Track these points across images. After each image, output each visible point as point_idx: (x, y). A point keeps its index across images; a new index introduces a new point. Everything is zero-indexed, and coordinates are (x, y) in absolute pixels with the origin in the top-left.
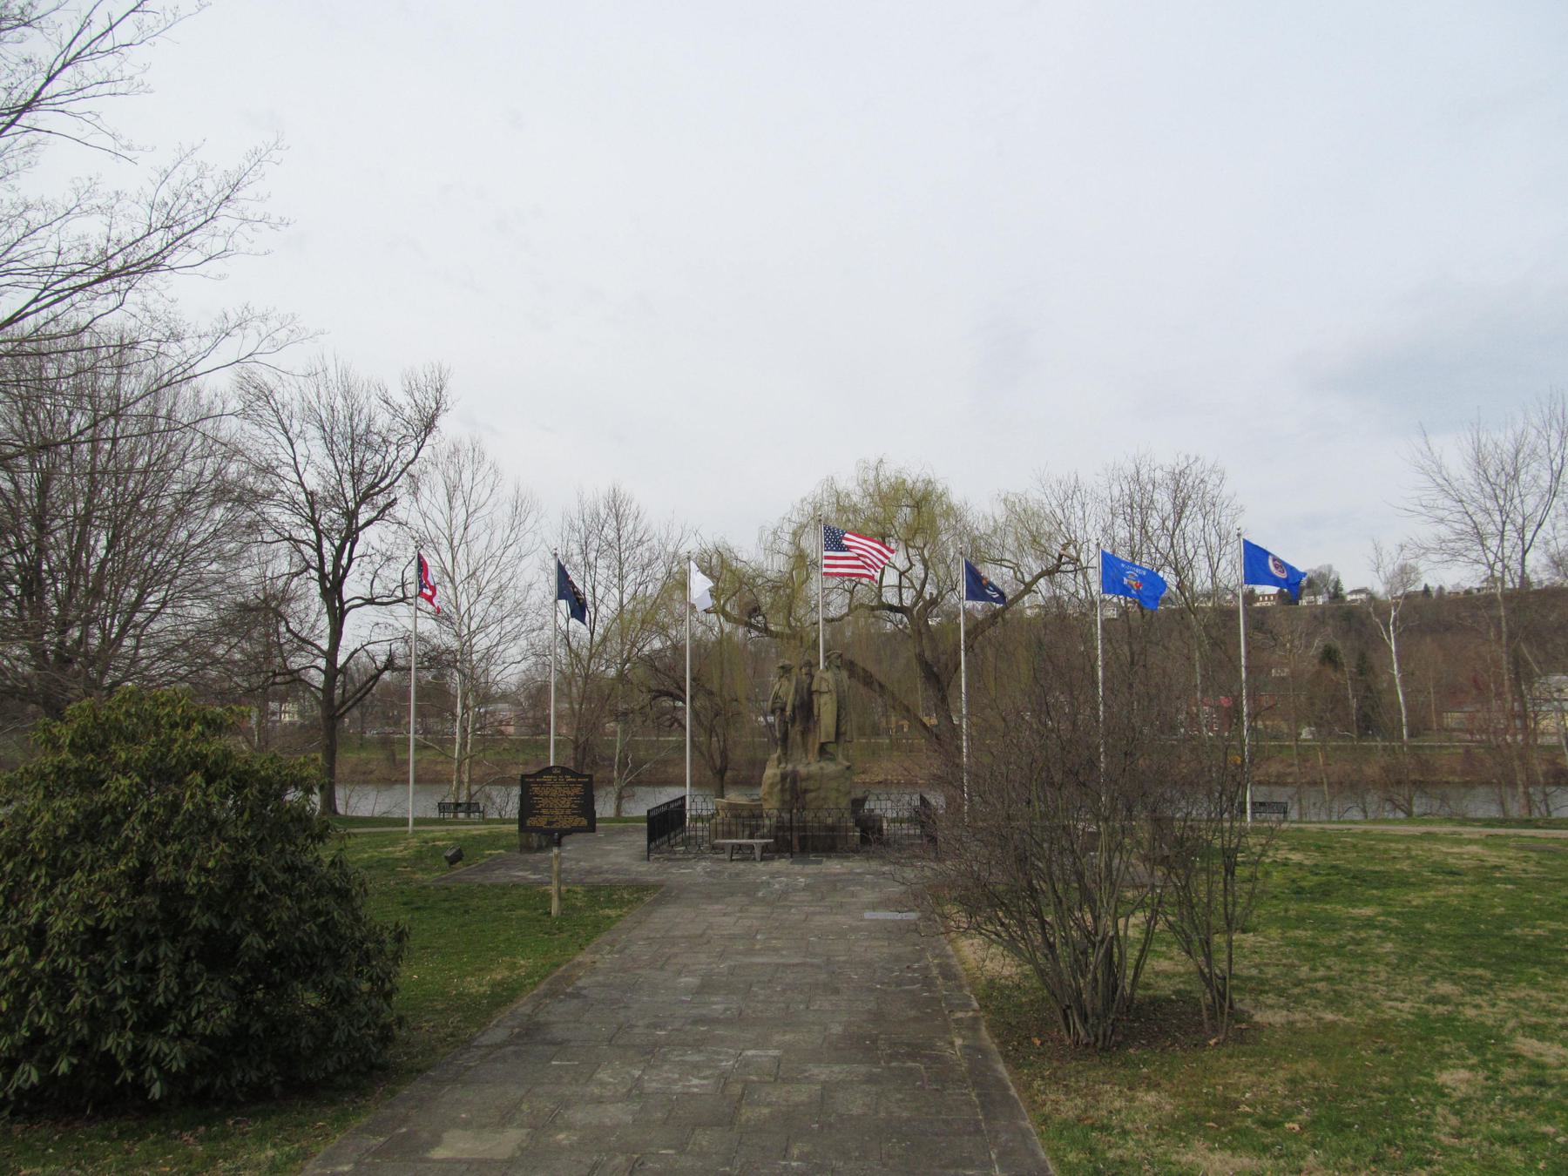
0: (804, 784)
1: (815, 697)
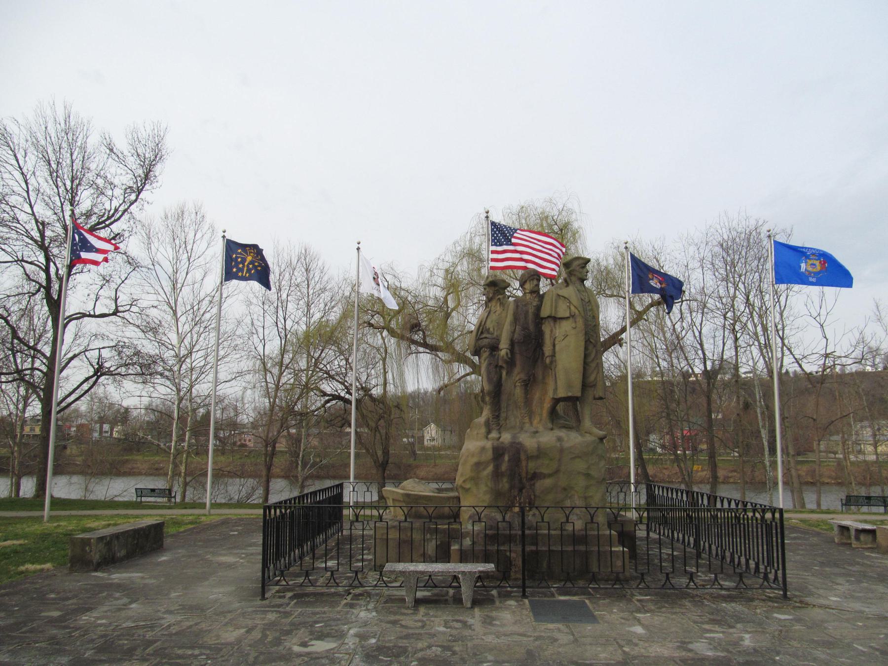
0: (532, 465)
1: (546, 328)
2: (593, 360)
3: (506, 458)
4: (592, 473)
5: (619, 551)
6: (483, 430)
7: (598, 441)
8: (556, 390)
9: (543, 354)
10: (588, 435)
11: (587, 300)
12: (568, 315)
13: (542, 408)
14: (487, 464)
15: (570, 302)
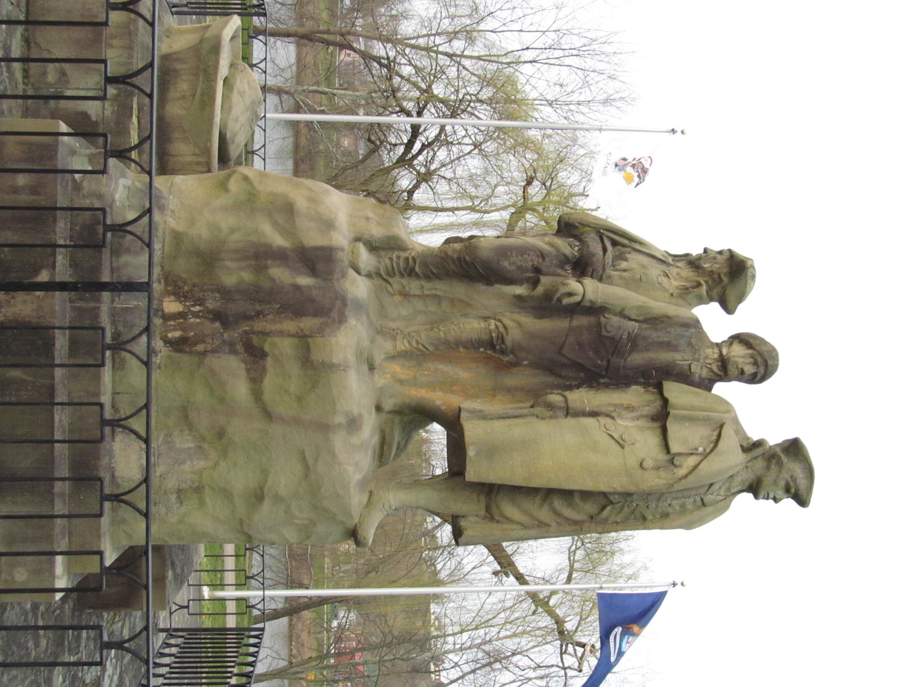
0: (284, 347)
1: (635, 396)
2: (556, 513)
3: (304, 281)
4: (267, 505)
5: (53, 576)
6: (377, 232)
7: (350, 524)
8: (483, 416)
9: (570, 388)
10: (365, 500)
11: (708, 498)
12: (675, 448)
13: (431, 386)
14: (289, 230)
15: (706, 455)
